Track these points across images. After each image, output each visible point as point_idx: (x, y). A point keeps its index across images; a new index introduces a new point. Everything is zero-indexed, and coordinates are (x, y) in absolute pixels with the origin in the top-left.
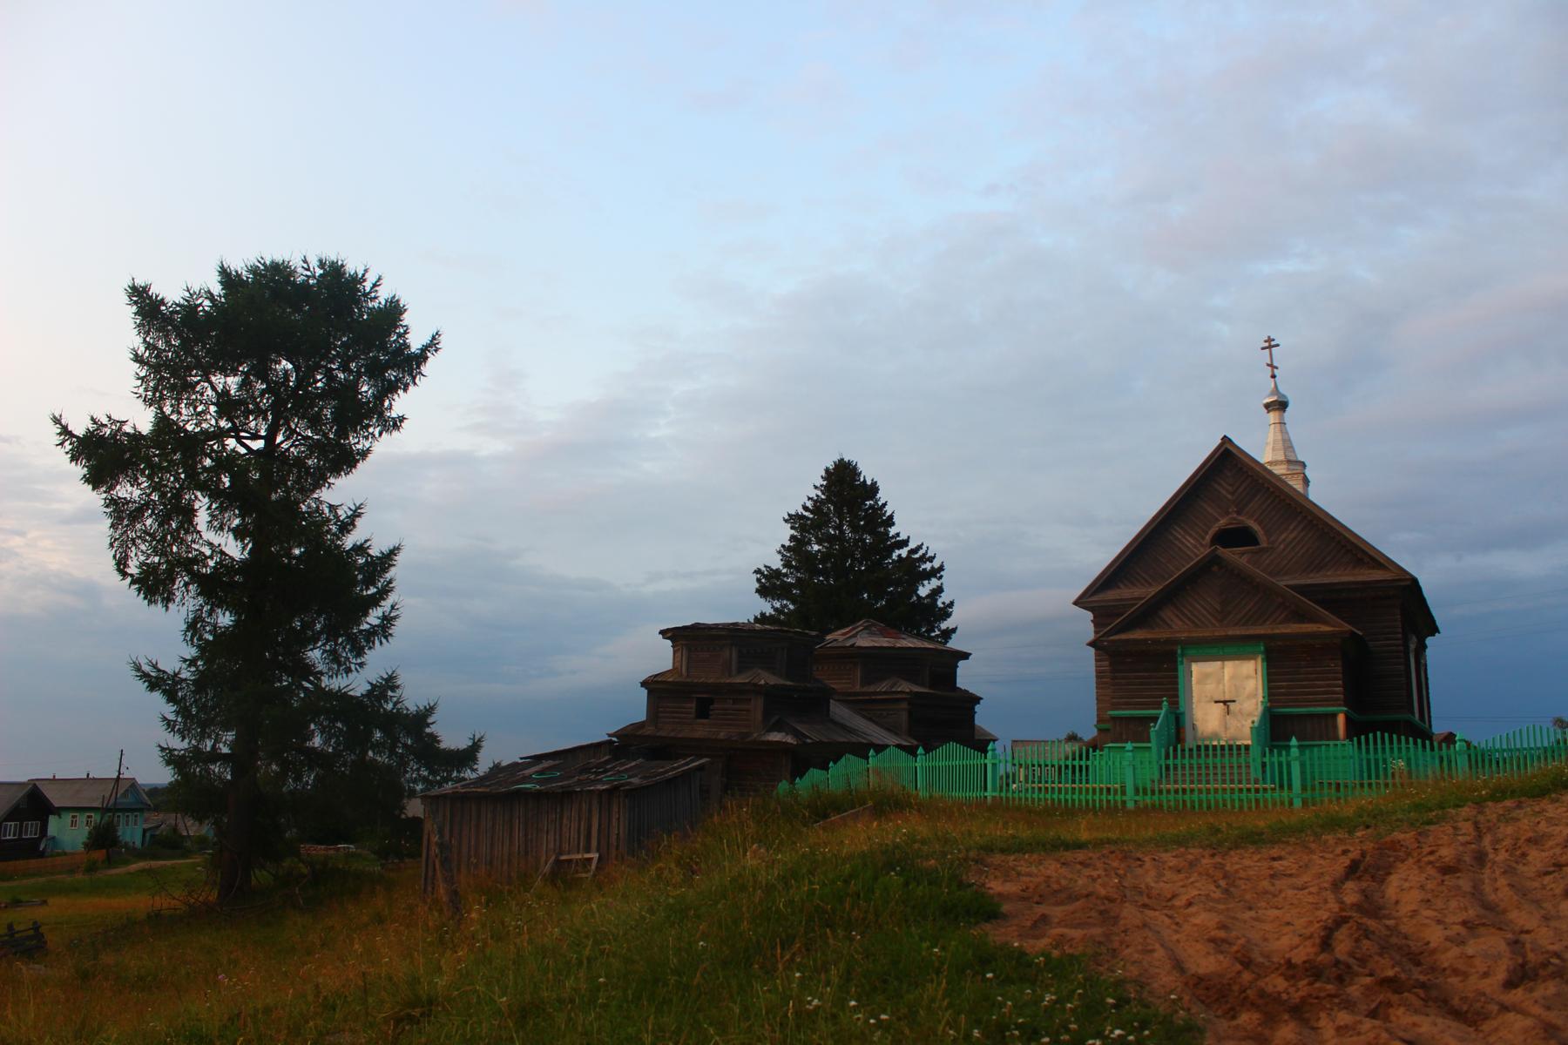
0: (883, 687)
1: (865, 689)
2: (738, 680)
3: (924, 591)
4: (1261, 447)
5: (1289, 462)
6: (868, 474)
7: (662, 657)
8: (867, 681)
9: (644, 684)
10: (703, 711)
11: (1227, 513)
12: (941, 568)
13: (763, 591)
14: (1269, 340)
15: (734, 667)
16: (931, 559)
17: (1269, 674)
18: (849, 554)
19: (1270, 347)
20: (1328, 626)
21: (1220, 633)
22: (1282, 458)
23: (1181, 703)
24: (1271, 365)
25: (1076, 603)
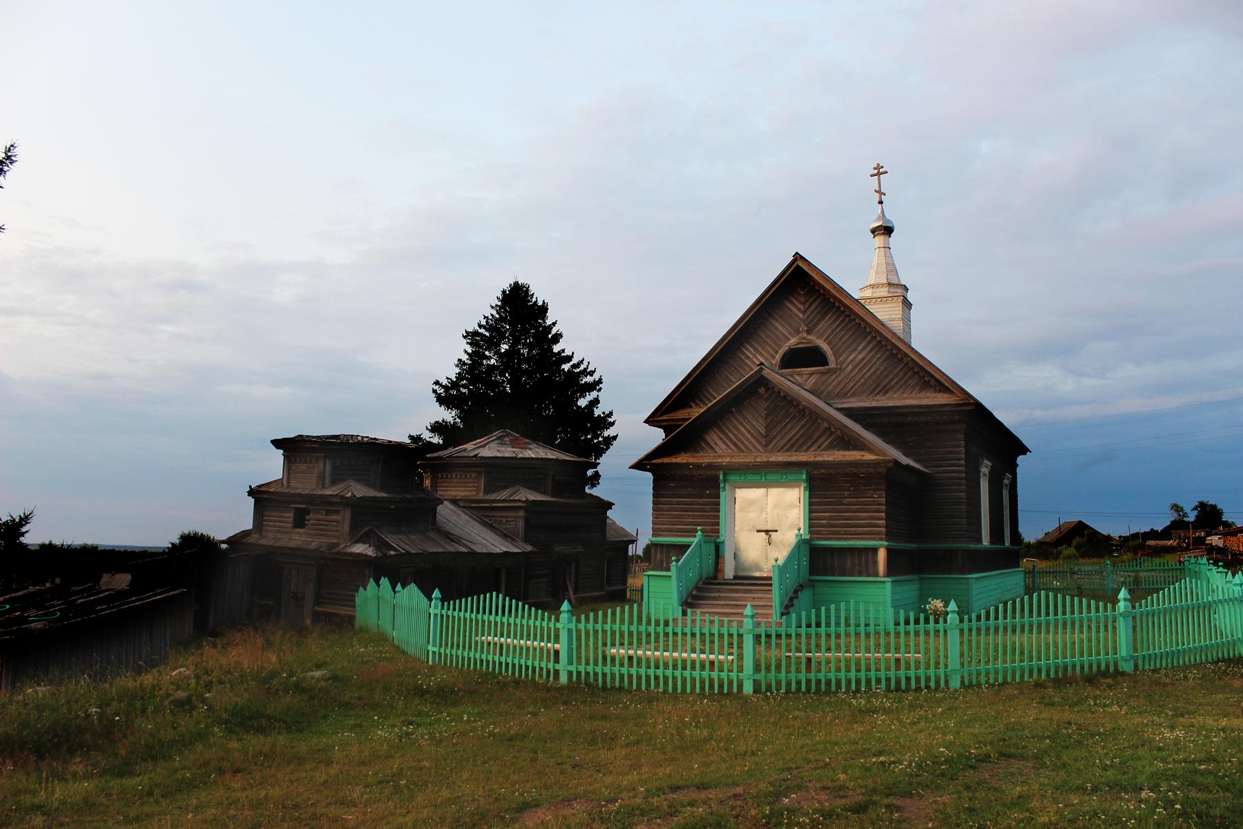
0: (504, 495)
1: (489, 497)
2: (328, 492)
3: (583, 403)
4: (853, 271)
5: (890, 284)
6: (539, 294)
7: (272, 467)
8: (488, 490)
9: (252, 492)
10: (300, 522)
11: (798, 332)
12: (600, 381)
13: (441, 400)
14: (878, 167)
15: (327, 480)
16: (591, 373)
17: (811, 504)
18: (520, 368)
19: (879, 174)
20: (881, 450)
21: (763, 458)
22: (885, 281)
23: (722, 531)
24: (879, 192)
25: (646, 422)
